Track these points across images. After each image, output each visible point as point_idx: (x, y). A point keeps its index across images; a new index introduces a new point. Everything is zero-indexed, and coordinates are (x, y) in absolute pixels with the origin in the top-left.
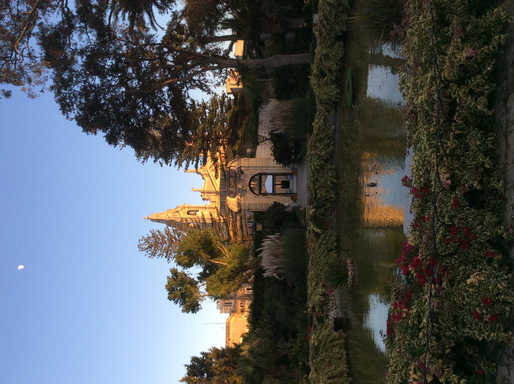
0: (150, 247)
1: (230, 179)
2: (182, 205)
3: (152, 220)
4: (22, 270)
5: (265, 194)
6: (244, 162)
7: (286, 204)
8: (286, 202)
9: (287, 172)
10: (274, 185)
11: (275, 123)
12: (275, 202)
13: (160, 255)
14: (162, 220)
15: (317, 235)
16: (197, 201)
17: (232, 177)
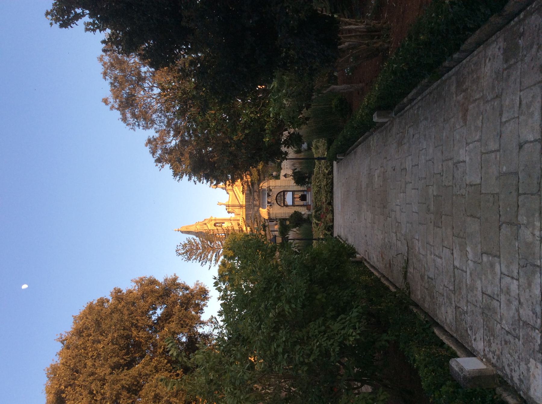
0: (186, 252)
1: (254, 193)
2: (209, 218)
3: (182, 232)
4: (27, 288)
5: (287, 206)
6: (272, 183)
7: (303, 213)
8: (303, 211)
9: (303, 189)
10: (293, 198)
11: (295, 165)
12: (295, 211)
13: (195, 259)
14: (192, 232)
15: (317, 224)
16: (222, 214)
17: (256, 192)
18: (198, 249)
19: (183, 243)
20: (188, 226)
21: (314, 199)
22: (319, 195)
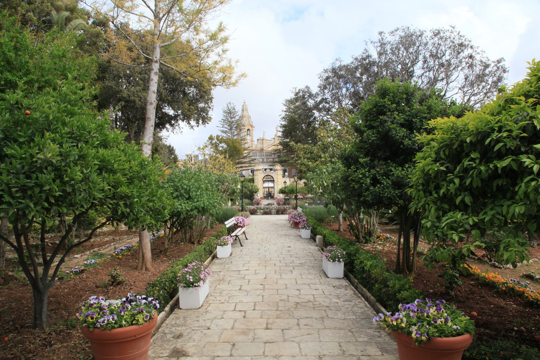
16: (256, 134)
18: (232, 118)
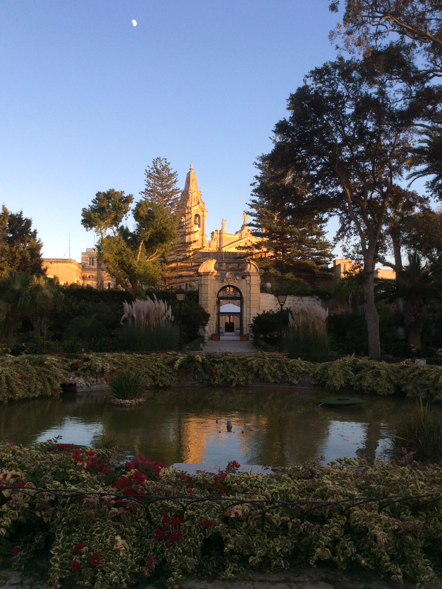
1: (236, 263)
2: (206, 208)
3: (189, 174)
4: (132, 25)
5: (218, 304)
7: (207, 328)
9: (244, 329)
10: (229, 314)
11: (300, 315)
12: (209, 315)
13: (149, 183)
14: (189, 186)
15: (171, 364)
17: (239, 266)
19: (170, 167)
20: (196, 182)
21: (230, 357)
22: (239, 371)
